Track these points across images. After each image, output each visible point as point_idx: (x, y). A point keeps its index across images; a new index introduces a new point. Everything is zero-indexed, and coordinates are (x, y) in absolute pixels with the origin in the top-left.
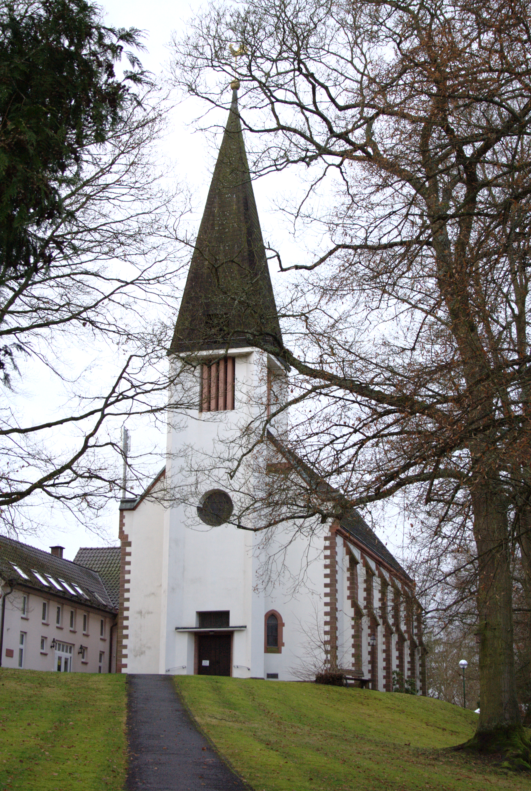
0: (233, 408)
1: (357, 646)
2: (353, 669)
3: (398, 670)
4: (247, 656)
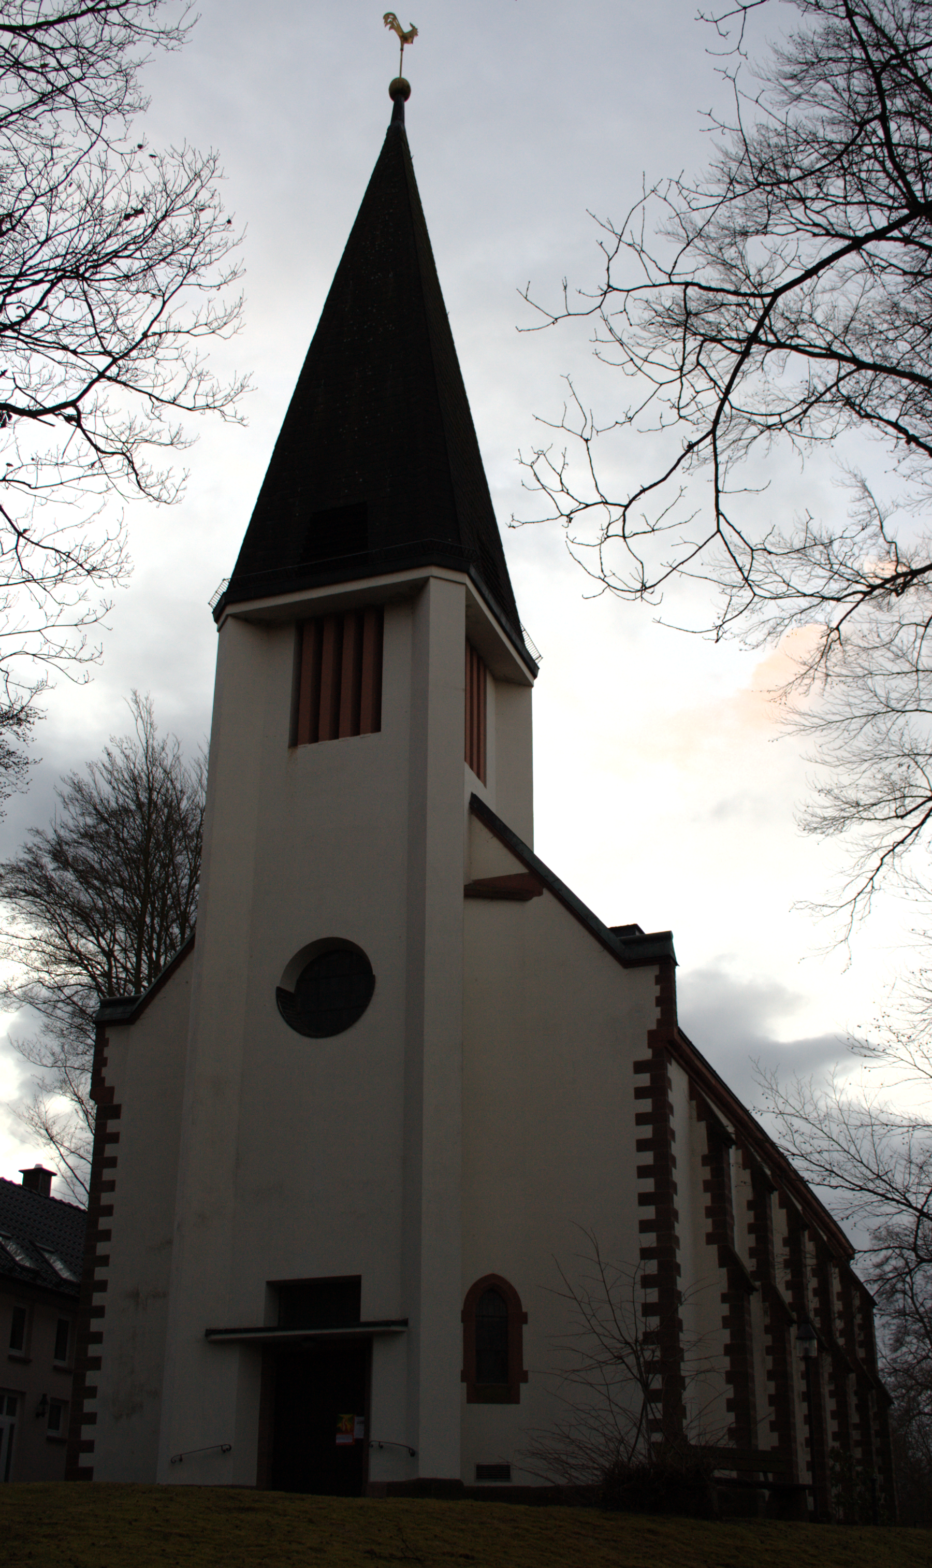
0: (377, 728)
1: (739, 1376)
2: (732, 1445)
3: (837, 1444)
4: (422, 1415)
